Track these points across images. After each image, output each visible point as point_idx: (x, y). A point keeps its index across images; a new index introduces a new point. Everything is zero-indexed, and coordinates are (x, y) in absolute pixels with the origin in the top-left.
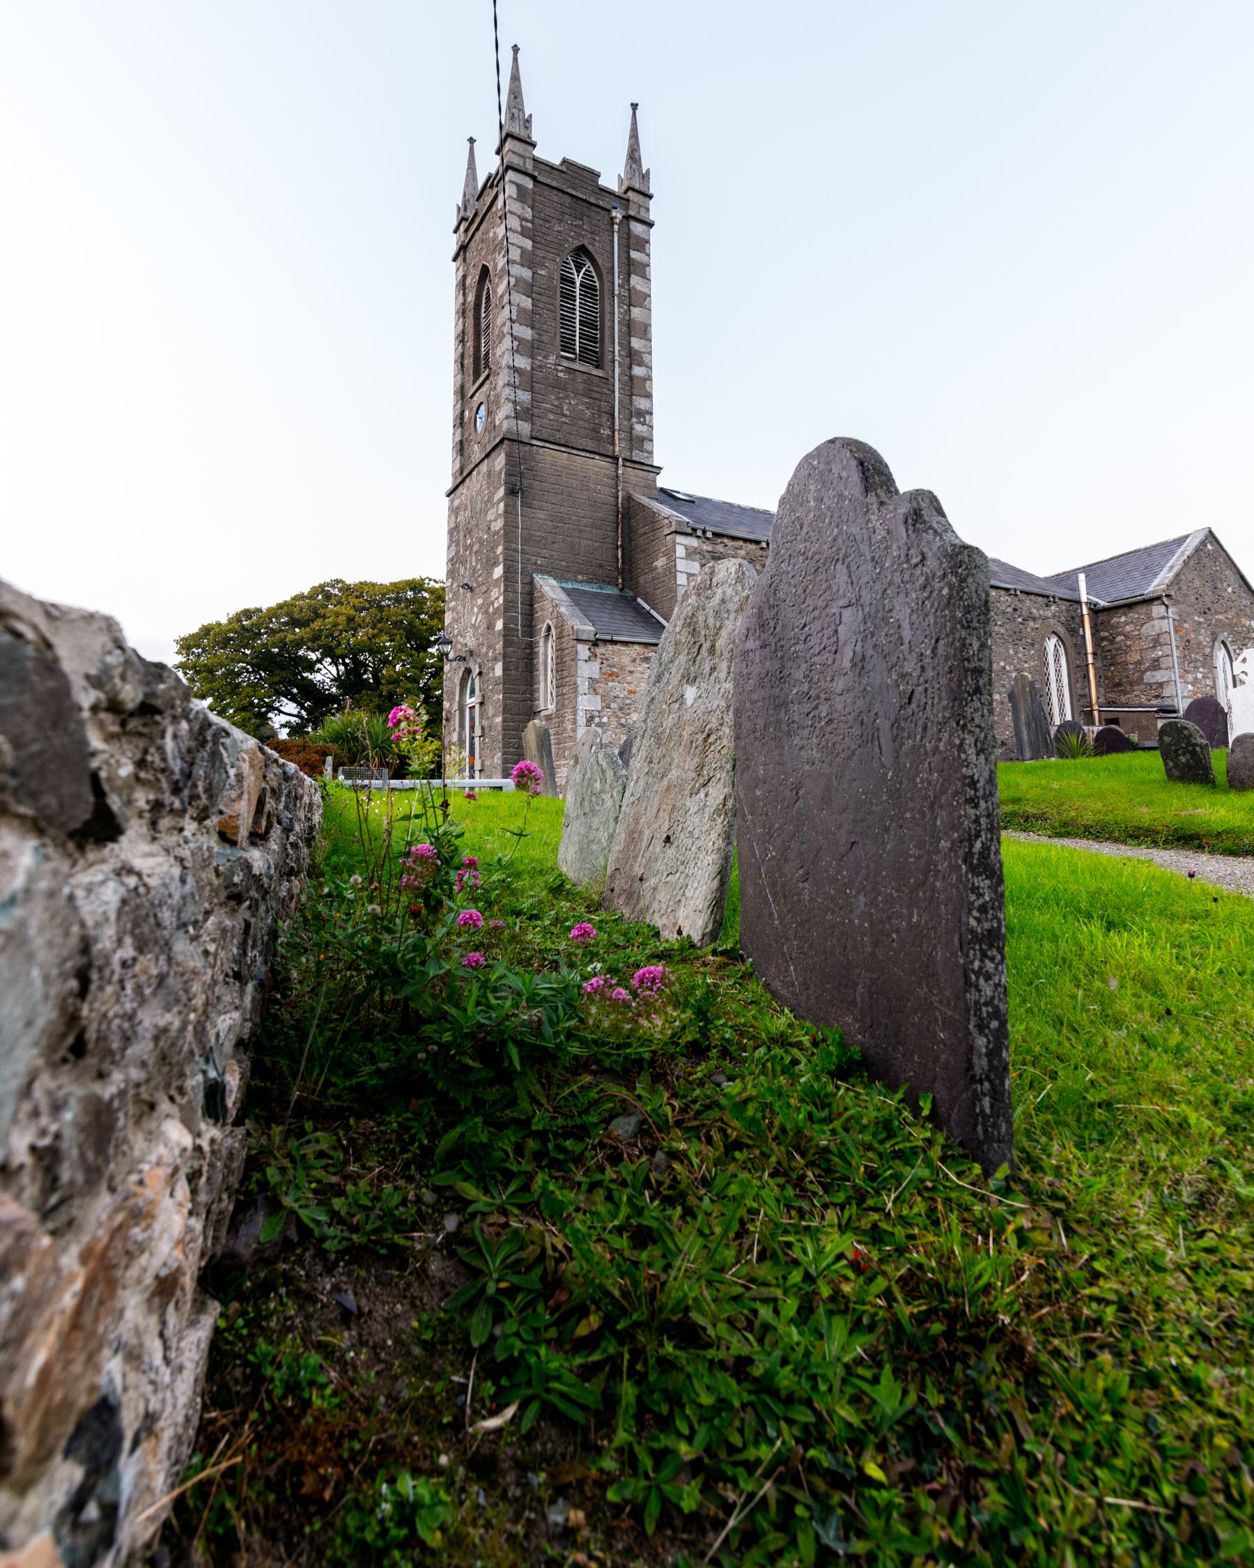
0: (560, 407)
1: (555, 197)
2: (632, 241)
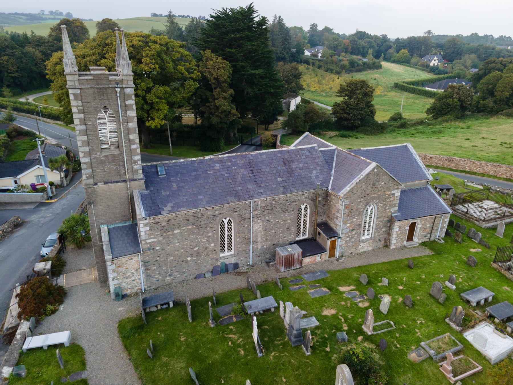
0: (104, 169)
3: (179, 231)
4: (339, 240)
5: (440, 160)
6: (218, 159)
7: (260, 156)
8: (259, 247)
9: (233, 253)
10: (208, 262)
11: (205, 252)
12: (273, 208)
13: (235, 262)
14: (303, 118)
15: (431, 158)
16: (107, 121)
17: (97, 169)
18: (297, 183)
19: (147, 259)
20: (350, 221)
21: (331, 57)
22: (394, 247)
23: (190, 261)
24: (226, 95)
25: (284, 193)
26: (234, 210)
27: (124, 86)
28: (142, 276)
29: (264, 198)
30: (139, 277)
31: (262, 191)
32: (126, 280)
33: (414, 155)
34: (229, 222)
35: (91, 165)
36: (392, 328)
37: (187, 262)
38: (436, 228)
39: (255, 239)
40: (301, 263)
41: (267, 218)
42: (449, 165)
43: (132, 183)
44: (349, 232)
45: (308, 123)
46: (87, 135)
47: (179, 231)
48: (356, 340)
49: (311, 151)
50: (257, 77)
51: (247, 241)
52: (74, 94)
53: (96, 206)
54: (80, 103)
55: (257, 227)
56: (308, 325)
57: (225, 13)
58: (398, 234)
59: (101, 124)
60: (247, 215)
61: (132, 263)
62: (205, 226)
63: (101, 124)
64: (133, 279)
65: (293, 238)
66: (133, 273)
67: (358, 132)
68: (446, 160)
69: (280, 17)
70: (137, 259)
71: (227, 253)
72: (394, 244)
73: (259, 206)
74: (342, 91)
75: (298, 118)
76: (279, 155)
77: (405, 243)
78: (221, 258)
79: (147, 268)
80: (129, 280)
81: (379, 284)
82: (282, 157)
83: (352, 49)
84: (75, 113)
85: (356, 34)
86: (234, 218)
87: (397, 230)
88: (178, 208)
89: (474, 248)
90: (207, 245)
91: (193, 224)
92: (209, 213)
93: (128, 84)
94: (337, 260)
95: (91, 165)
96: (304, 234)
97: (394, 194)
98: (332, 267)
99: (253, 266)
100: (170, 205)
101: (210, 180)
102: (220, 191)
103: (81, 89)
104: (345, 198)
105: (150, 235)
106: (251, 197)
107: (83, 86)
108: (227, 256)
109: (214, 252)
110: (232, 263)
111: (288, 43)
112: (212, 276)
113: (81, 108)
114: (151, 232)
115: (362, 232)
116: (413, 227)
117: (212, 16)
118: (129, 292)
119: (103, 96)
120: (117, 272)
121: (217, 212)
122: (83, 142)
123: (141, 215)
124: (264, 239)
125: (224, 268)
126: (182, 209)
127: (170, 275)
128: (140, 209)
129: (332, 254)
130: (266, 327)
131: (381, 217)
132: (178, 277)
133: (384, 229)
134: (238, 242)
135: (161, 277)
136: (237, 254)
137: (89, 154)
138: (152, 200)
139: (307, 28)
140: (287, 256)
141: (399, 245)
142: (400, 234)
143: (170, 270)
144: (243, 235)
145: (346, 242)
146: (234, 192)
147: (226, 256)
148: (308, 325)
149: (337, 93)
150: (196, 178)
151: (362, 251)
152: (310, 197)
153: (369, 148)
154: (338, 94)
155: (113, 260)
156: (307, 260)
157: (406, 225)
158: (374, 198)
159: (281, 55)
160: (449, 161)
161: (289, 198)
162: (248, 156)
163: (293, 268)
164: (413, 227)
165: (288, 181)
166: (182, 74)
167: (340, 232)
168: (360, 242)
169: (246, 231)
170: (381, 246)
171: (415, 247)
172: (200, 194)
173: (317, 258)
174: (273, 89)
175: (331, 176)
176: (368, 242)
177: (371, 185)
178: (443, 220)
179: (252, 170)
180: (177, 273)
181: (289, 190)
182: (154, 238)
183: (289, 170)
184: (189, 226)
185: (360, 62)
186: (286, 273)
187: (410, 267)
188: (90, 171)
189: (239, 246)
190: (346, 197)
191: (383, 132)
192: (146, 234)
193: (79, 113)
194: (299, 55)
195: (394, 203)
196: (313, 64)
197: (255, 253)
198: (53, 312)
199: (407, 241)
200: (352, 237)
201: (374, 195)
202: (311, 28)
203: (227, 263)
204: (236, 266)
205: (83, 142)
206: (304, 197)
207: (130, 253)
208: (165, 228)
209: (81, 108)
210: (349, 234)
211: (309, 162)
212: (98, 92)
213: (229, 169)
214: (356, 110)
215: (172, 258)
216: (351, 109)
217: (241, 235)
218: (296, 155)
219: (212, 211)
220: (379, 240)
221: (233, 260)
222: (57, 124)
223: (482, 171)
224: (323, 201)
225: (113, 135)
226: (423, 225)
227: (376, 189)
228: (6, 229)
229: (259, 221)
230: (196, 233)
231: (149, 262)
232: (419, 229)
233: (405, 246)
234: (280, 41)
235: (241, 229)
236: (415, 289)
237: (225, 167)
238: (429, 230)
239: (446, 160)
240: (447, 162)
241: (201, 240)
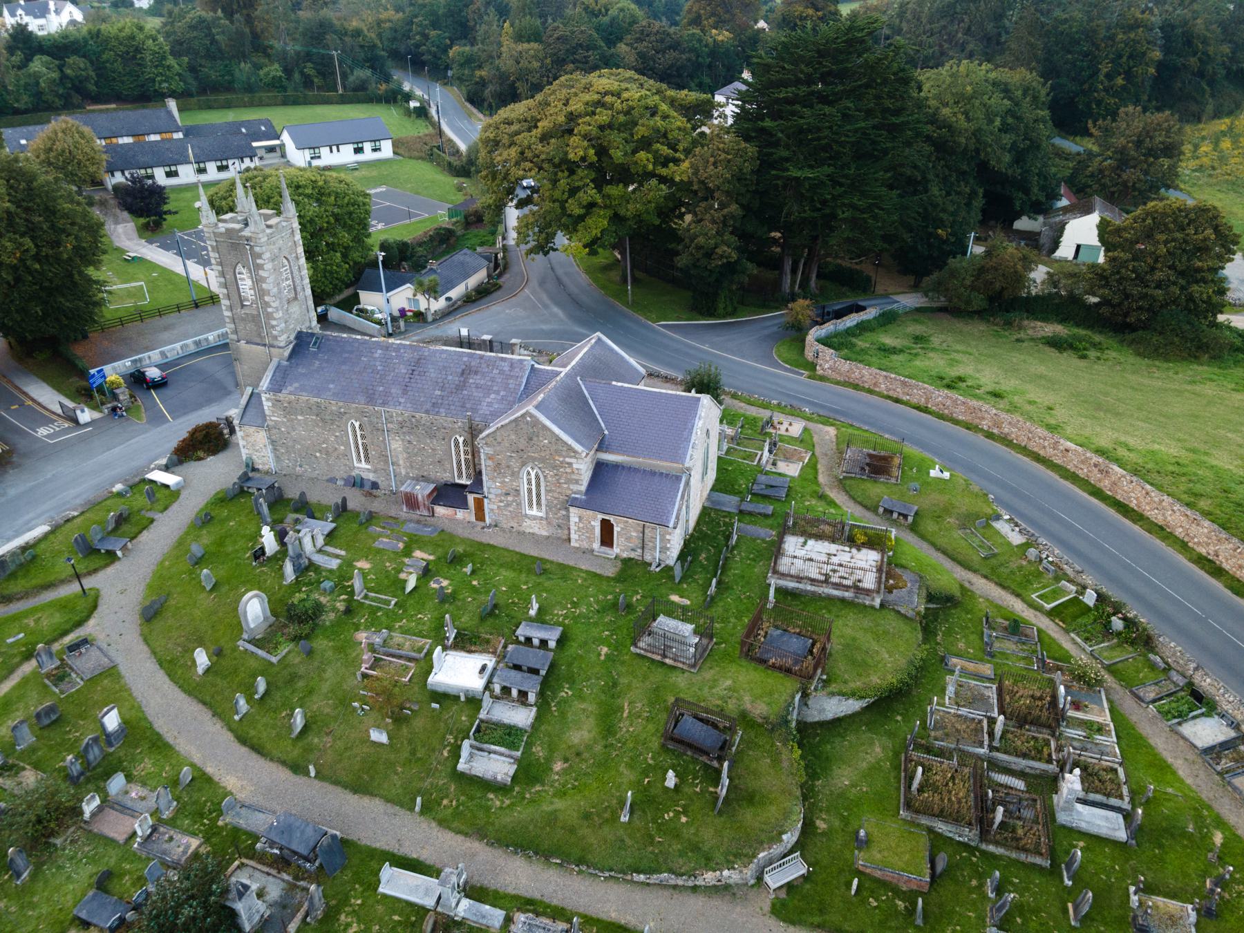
5: (1083, 462)
11: (335, 454)
15: (1067, 450)
29: (399, 410)
42: (1100, 481)
51: (384, 457)
68: (1096, 466)
77: (596, 545)
87: (577, 520)
97: (570, 464)
100: (296, 385)
101: (357, 369)
106: (384, 404)
108: (362, 468)
116: (607, 528)
118: (260, 467)
129: (480, 515)
137: (231, 308)
141: (585, 545)
153: (626, 385)
156: (440, 510)
158: (534, 459)
160: (1101, 471)
164: (607, 528)
172: (333, 382)
173: (460, 514)
188: (233, 326)
191: (1196, 357)
198: (200, 459)
200: (508, 505)
204: (375, 485)
221: (372, 477)
223: (1160, 520)
238: (638, 542)
239: (1096, 466)
240: (1096, 470)
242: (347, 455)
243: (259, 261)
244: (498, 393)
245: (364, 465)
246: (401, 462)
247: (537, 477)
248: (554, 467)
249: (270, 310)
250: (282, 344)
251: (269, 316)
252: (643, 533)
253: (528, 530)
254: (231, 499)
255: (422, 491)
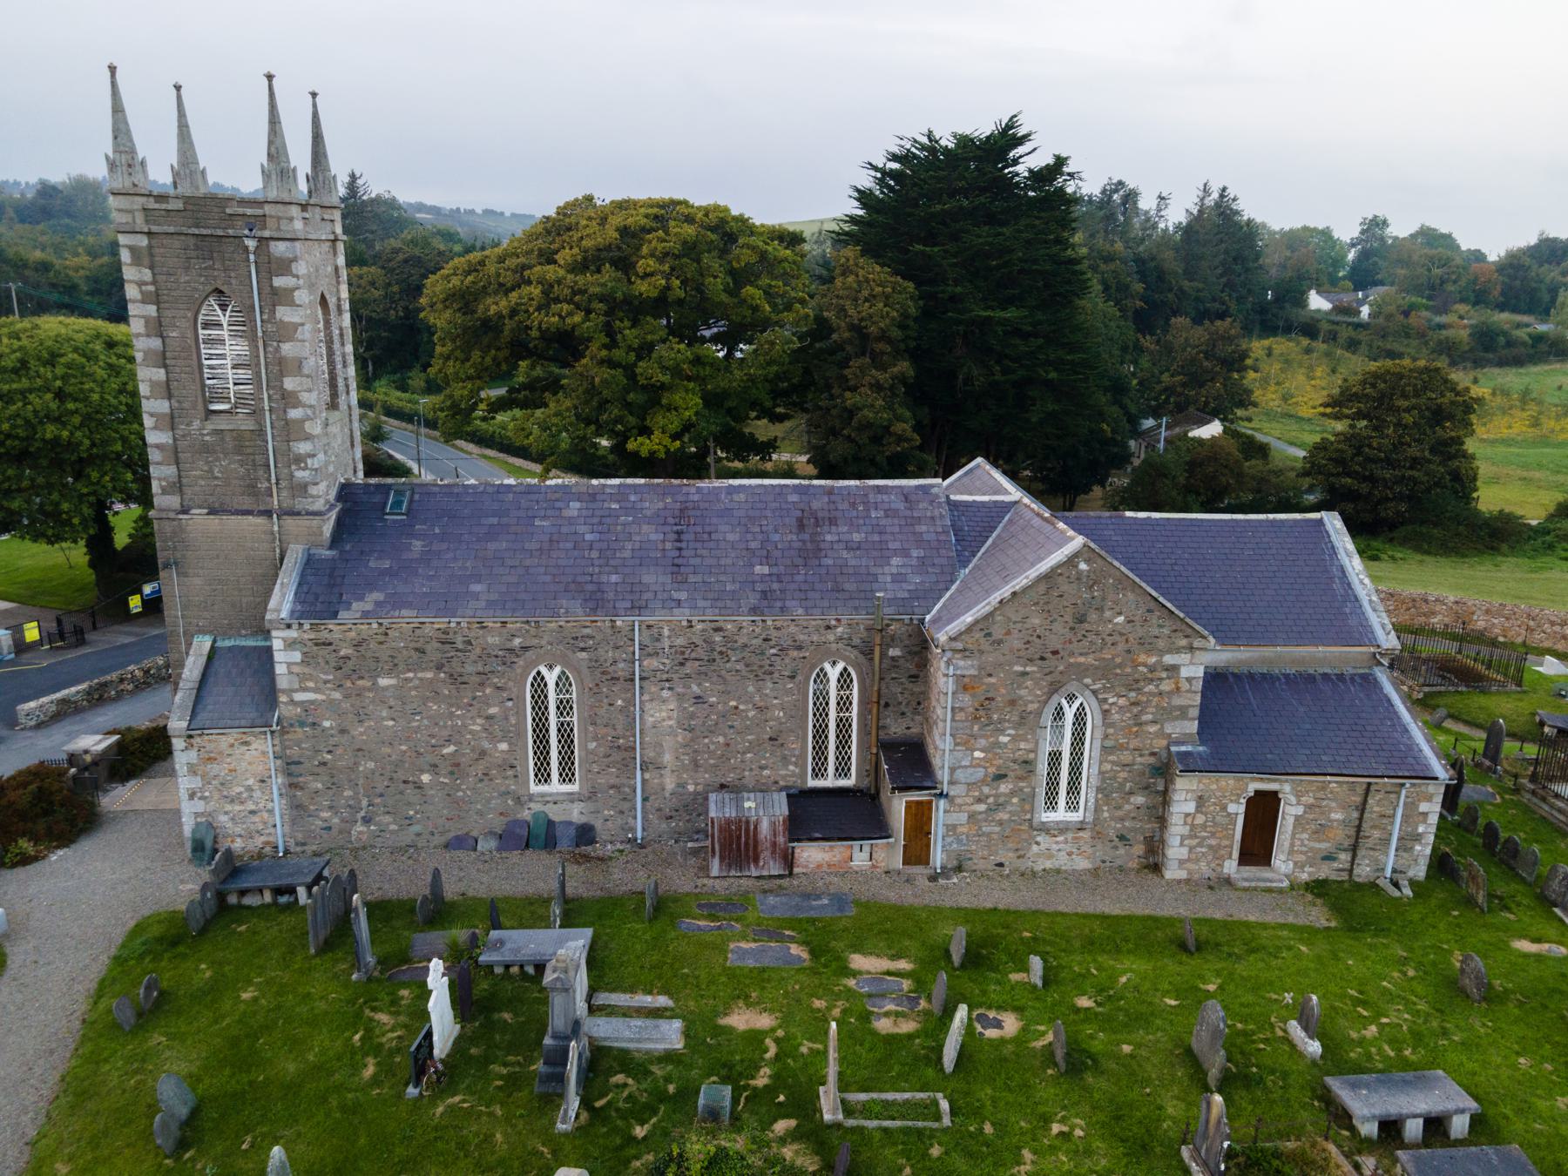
0: (211, 471)
1: (177, 243)
2: (274, 266)
3: (393, 682)
4: (942, 803)
6: (584, 489)
7: (729, 493)
8: (670, 783)
9: (573, 788)
10: (488, 801)
11: (480, 768)
12: (717, 657)
13: (583, 820)
14: (1182, 480)
16: (225, 334)
17: (193, 469)
18: (818, 586)
19: (294, 752)
20: (983, 742)
21: (1406, 314)
22: (1183, 875)
23: (431, 785)
24: (882, 377)
25: (754, 610)
26: (576, 643)
27: (267, 234)
28: (278, 805)
29: (681, 616)
30: (270, 805)
31: (683, 596)
32: (228, 807)
33: (1342, 555)
34: (563, 682)
35: (174, 454)
36: (936, 1125)
37: (419, 786)
38: (1376, 834)
39: (652, 754)
40: (789, 861)
41: (695, 688)
43: (289, 522)
44: (983, 781)
45: (1198, 494)
46: (165, 366)
47: (393, 682)
48: (767, 1125)
49: (913, 497)
50: (999, 330)
51: (621, 754)
52: (132, 249)
53: (186, 575)
54: (147, 275)
55: (660, 714)
56: (639, 1041)
57: (932, 147)
58: (1193, 826)
59: (210, 341)
60: (621, 665)
61: (247, 757)
62: (477, 679)
63: (210, 341)
64: (253, 807)
65: (793, 775)
66: (249, 789)
67: (1391, 540)
69: (1224, 189)
70: (263, 748)
71: (556, 786)
72: (1181, 862)
73: (666, 643)
74: (1338, 404)
75: (1165, 476)
76: (794, 498)
77: (1231, 867)
78: (531, 798)
79: (295, 780)
80: (238, 808)
81: (1015, 977)
82: (802, 506)
83: (1503, 293)
84: (134, 301)
85: (1536, 247)
86: (576, 671)
87: (1190, 807)
88: (394, 608)
89: (1537, 940)
90: (486, 745)
91: (439, 667)
92: (490, 640)
93: (278, 229)
94: (933, 878)
95: (174, 454)
96: (843, 770)
97: (1173, 669)
98: (905, 896)
99: (642, 846)
102: (548, 578)
103: (149, 234)
104: (955, 651)
105: (303, 678)
106: (637, 608)
107: (155, 229)
108: (556, 795)
109: (510, 773)
110: (570, 823)
111: (1247, 270)
112: (499, 849)
113: (151, 288)
114: (306, 670)
115: (1041, 792)
116: (1263, 811)
117: (894, 158)
119: (212, 258)
120: (203, 777)
121: (517, 642)
122: (154, 384)
123: (278, 611)
124: (686, 760)
125: (542, 831)
126: (404, 612)
127: (367, 821)
128: (283, 595)
129: (917, 852)
130: (507, 1016)
131: (1122, 748)
132: (392, 832)
133: (1139, 800)
134: (592, 752)
135: (336, 820)
136: (590, 796)
137: (171, 421)
138: (331, 576)
139: (1347, 231)
140: (728, 822)
141: (1204, 869)
142: (1204, 826)
143: (365, 803)
144: (609, 730)
145: (972, 816)
146: (590, 587)
147: (551, 795)
148: (639, 1041)
149: (1325, 405)
150: (492, 534)
151: (1048, 865)
152: (856, 641)
154: (1329, 410)
155: (190, 737)
156: (812, 855)
157: (1232, 796)
158: (1081, 671)
159: (1217, 305)
161: (774, 633)
162: (685, 490)
163: (755, 873)
164: (1263, 811)
165: (786, 579)
166: (755, 309)
167: (943, 775)
168: (1031, 826)
169: (620, 721)
170: (1134, 864)
171: (1270, 890)
172: (478, 578)
173: (860, 856)
174: (1056, 369)
175: (952, 582)
176: (1070, 835)
177: (1068, 618)
178: (1411, 807)
179: (678, 533)
180: (388, 818)
181: (779, 604)
182: (316, 690)
183: (809, 545)
184: (423, 670)
185: (1521, 334)
186: (726, 883)
187: (1183, 947)
189: (595, 768)
190: (959, 645)
191: (1492, 548)
192: (290, 673)
193: (143, 302)
194: (1282, 308)
195: (1177, 701)
196: (1332, 337)
197: (655, 802)
198: (25, 860)
199: (1240, 863)
200: (999, 806)
201: (1082, 659)
202: (1363, 232)
203: (556, 819)
204: (585, 834)
205: (154, 384)
206: (831, 638)
207: (243, 723)
208: (350, 664)
209: (151, 288)
210: (986, 790)
211: (889, 529)
212: (197, 248)
213: (608, 520)
214: (1389, 463)
215: (371, 765)
216: (1369, 460)
217: (602, 731)
218: (853, 505)
219: (500, 635)
220: (1122, 838)
221: (576, 814)
222: (485, 457)
224: (899, 662)
225: (244, 374)
226: (1309, 807)
227: (1091, 637)
228: (159, 669)
229: (665, 694)
230: (449, 696)
231: (299, 763)
232: (1290, 821)
233: (1228, 881)
234: (1217, 262)
235: (602, 712)
236: (1141, 1019)
237: (598, 513)
238: (1342, 835)
241: (465, 726)
242: (510, 766)
243: (278, 282)
244: (905, 553)
245: (556, 786)
246: (667, 758)
247: (1080, 718)
248: (1134, 684)
249: (294, 414)
250: (319, 505)
251: (291, 432)
252: (1362, 808)
253: (1039, 867)
254: (203, 931)
255: (767, 813)
